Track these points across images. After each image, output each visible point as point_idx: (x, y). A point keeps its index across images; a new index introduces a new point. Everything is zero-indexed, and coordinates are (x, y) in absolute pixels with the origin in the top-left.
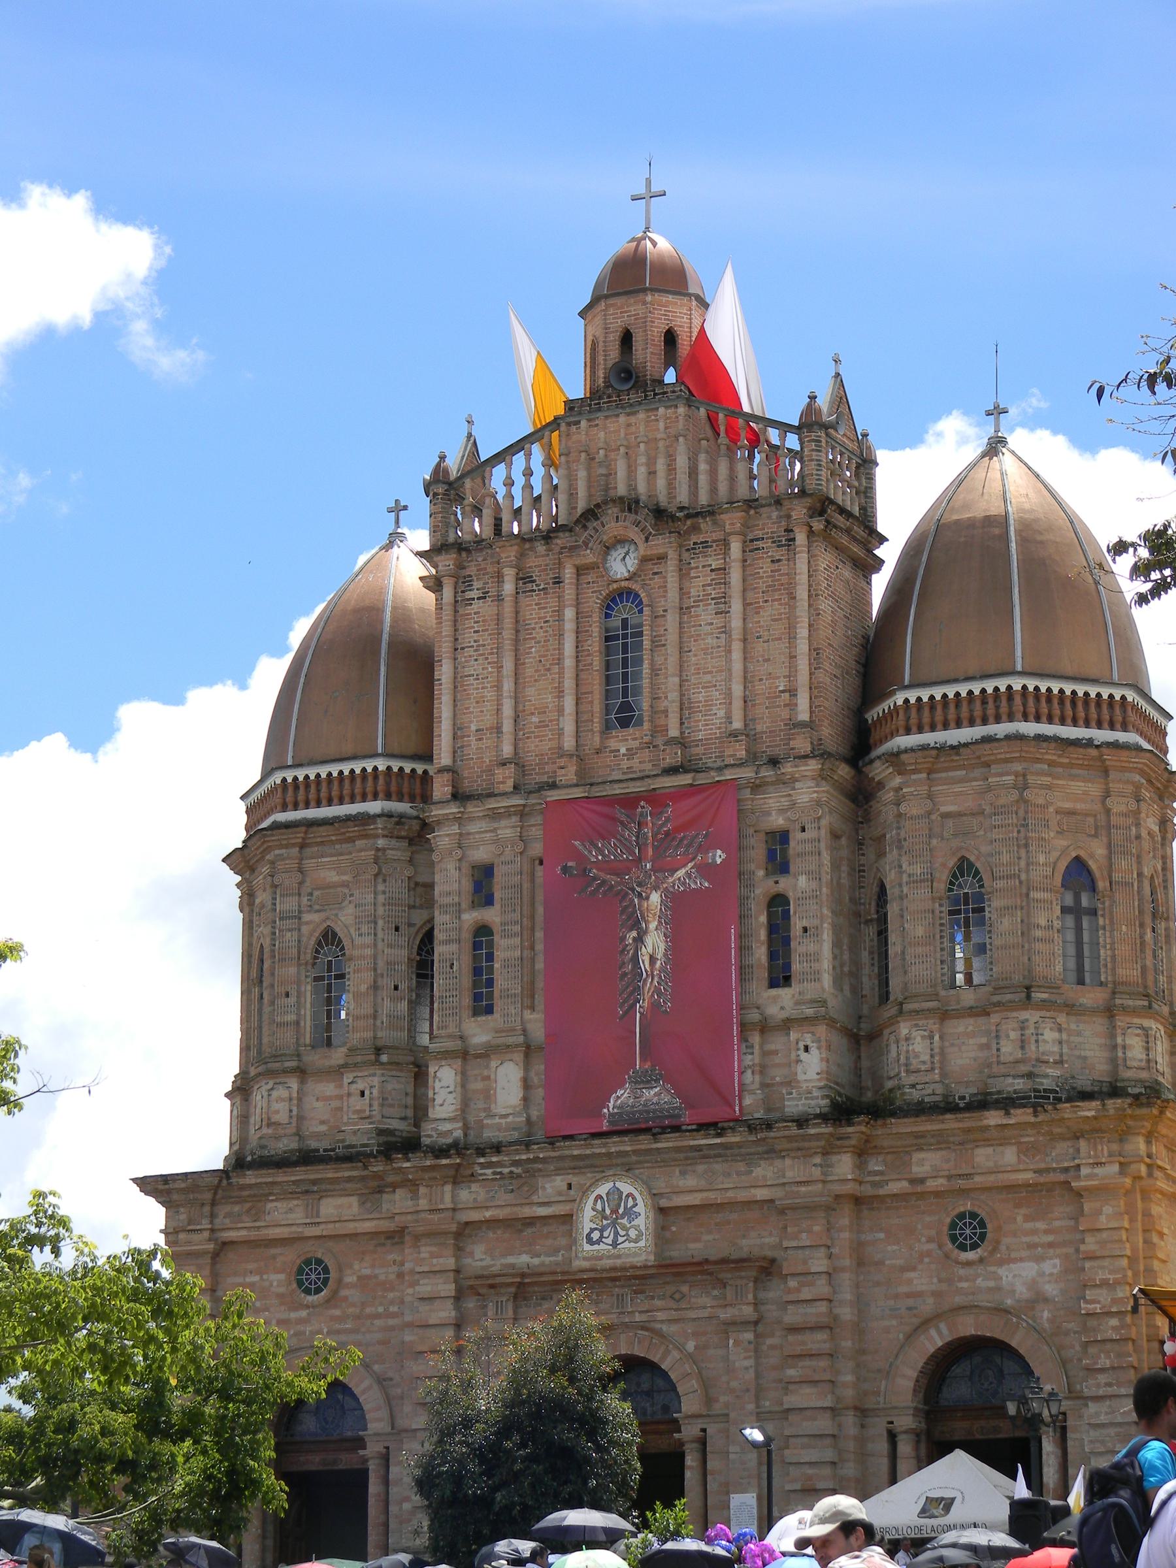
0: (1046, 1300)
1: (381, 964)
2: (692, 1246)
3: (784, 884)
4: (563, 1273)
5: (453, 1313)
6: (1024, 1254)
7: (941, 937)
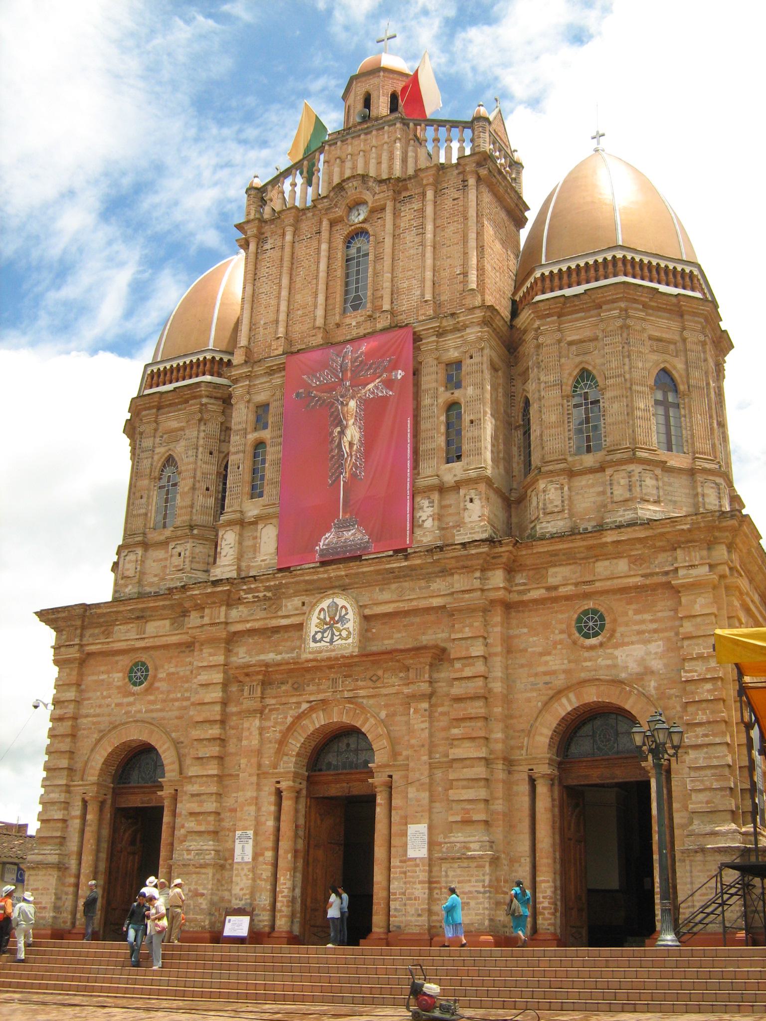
0: (652, 672)
1: (199, 474)
2: (386, 642)
3: (458, 394)
4: (294, 663)
5: (220, 694)
6: (634, 638)
7: (569, 422)
